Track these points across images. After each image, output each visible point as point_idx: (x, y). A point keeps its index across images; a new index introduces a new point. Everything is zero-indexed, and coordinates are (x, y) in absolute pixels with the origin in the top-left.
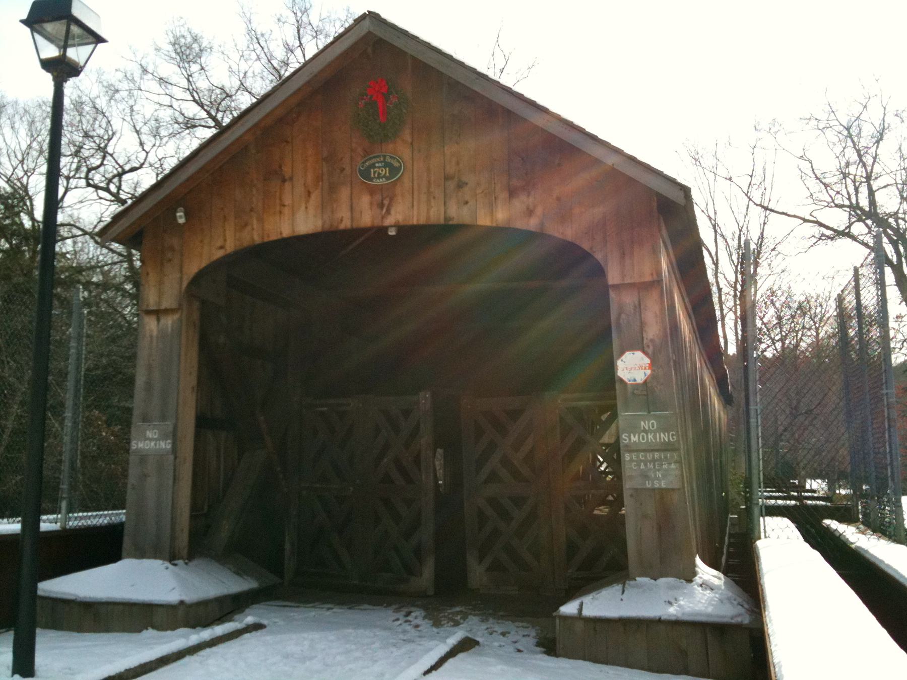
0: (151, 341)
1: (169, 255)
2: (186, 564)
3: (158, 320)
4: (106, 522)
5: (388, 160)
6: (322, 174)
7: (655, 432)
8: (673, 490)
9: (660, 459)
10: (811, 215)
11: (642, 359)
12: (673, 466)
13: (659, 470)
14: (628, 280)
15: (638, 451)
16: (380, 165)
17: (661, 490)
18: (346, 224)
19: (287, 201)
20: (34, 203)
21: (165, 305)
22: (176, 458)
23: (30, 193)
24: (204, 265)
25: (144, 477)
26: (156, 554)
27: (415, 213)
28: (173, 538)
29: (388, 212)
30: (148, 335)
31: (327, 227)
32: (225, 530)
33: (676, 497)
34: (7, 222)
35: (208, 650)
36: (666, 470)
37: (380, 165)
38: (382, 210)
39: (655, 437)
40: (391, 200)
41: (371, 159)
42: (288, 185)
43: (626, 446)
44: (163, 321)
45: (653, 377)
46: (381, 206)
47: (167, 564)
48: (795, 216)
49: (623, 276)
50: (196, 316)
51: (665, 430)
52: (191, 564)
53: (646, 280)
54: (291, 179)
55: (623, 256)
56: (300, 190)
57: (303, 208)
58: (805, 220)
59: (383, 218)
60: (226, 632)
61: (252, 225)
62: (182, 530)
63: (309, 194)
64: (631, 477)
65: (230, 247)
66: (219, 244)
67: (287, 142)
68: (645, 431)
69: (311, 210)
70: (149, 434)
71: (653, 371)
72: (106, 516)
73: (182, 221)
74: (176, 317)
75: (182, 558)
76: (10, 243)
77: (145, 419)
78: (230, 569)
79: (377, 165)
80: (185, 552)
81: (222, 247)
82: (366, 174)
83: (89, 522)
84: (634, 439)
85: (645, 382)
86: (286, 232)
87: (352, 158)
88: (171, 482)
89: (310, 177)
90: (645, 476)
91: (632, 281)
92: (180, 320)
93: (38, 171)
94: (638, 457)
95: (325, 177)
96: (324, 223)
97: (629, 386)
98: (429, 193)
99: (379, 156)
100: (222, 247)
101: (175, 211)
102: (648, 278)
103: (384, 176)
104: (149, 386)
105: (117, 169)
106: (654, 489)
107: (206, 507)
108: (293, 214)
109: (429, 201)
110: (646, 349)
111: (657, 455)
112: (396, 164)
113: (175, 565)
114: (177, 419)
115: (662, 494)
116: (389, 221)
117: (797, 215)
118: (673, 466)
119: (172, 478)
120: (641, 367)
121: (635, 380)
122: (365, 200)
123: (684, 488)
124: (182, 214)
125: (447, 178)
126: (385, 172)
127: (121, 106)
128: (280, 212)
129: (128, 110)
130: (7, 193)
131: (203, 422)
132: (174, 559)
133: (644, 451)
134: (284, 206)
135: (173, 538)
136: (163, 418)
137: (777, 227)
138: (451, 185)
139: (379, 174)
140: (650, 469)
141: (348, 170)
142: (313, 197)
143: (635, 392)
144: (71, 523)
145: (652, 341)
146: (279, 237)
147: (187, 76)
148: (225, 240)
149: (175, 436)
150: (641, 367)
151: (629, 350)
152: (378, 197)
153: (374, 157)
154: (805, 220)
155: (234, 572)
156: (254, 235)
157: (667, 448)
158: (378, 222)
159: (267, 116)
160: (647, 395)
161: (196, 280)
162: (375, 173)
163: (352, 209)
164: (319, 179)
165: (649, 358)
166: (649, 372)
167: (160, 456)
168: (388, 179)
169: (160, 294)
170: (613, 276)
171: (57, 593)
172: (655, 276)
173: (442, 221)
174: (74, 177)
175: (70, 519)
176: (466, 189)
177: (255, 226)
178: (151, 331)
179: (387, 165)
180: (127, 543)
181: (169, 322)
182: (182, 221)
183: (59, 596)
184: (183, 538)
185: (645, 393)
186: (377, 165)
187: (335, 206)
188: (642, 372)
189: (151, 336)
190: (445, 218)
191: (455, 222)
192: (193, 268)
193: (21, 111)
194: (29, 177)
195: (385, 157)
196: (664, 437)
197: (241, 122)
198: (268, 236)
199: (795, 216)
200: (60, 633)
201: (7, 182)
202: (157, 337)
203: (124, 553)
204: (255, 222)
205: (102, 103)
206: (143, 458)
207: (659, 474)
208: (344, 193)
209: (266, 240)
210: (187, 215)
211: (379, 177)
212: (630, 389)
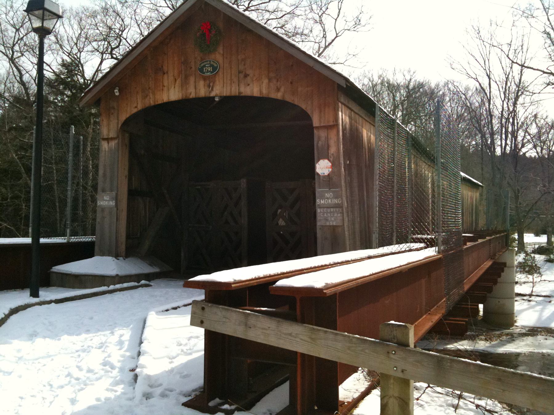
0: (105, 154)
1: (112, 111)
2: (124, 259)
3: (108, 143)
4: (90, 240)
5: (212, 63)
6: (182, 71)
7: (332, 199)
8: (339, 226)
9: (333, 212)
10: (547, 69)
11: (328, 163)
12: (339, 215)
13: (333, 217)
14: (322, 125)
15: (324, 208)
16: (208, 65)
17: (333, 226)
18: (193, 96)
19: (166, 84)
20: (84, 68)
21: (111, 135)
22: (117, 209)
23: (82, 62)
24: (128, 116)
25: (103, 218)
26: (109, 254)
27: (225, 90)
28: (117, 247)
29: (212, 89)
30: (104, 150)
31: (184, 97)
32: (146, 245)
33: (340, 229)
34: (69, 79)
35: (118, 292)
36: (336, 217)
37: (208, 65)
38: (209, 88)
39: (332, 201)
40: (214, 83)
41: (203, 62)
42: (166, 76)
43: (319, 205)
44: (110, 144)
45: (332, 172)
46: (209, 86)
47: (114, 259)
48: (538, 70)
49: (320, 122)
50: (127, 141)
51: (336, 198)
52: (126, 259)
53: (331, 124)
54: (167, 72)
55: (320, 112)
56: (171, 78)
57: (173, 87)
58: (544, 72)
59: (210, 92)
60: (129, 286)
61: (150, 96)
62: (122, 243)
63: (176, 80)
64: (320, 220)
65: (140, 107)
66: (135, 105)
67: (165, 54)
68: (327, 198)
69: (177, 87)
70: (105, 198)
71: (332, 169)
72: (90, 238)
73: (117, 94)
74: (116, 141)
75: (122, 257)
76: (71, 92)
77: (104, 191)
78: (147, 263)
79: (207, 66)
80: (124, 254)
81: (136, 107)
82: (201, 70)
83: (81, 240)
84: (322, 202)
85: (329, 174)
86: (165, 100)
87: (195, 62)
88: (115, 221)
89: (176, 71)
90: (327, 220)
91: (325, 125)
92: (118, 143)
93: (85, 49)
94: (324, 211)
95: (183, 72)
96: (183, 95)
97: (321, 177)
98: (231, 80)
99: (207, 61)
100: (136, 107)
101: (115, 89)
102: (331, 123)
103: (210, 71)
104: (104, 175)
105: (128, 48)
106: (330, 226)
107: (139, 234)
108: (168, 90)
109: (231, 84)
110: (330, 158)
111: (332, 210)
112: (215, 65)
113: (118, 259)
114: (117, 191)
115: (334, 228)
116: (213, 94)
117: (539, 69)
118: (339, 215)
119: (115, 219)
120: (327, 168)
121: (324, 174)
122: (202, 83)
123: (344, 225)
124: (117, 91)
125: (240, 72)
126: (210, 69)
127: (129, 10)
128: (163, 90)
129: (133, 12)
130: (68, 63)
131: (132, 194)
132: (118, 257)
133: (327, 208)
134: (164, 86)
135: (117, 247)
136: (111, 191)
137: (528, 76)
138: (242, 76)
139: (208, 70)
140: (329, 216)
141: (193, 68)
142: (177, 82)
143: (324, 179)
144: (72, 240)
145: (333, 154)
146: (162, 102)
147: (143, 4)
148: (138, 104)
149: (116, 199)
150: (327, 168)
151: (322, 159)
152: (208, 82)
153: (205, 62)
154: (544, 72)
155: (149, 264)
156: (151, 101)
157: (339, 206)
158: (207, 95)
159: (154, 41)
160: (329, 181)
161: (126, 123)
162: (205, 70)
163: (195, 88)
164: (180, 73)
165: (331, 163)
166: (330, 170)
167: (111, 208)
168: (212, 72)
169: (109, 131)
170: (316, 123)
171: (63, 271)
172: (335, 122)
173: (237, 94)
174: (105, 53)
175: (71, 239)
176: (249, 78)
177: (151, 97)
178: (105, 148)
179: (212, 66)
180: (96, 248)
181: (113, 144)
182: (117, 94)
183: (64, 272)
184: (123, 247)
185: (328, 180)
186: (207, 66)
187: (187, 86)
188: (327, 170)
189: (105, 151)
190: (239, 93)
191: (243, 95)
192: (123, 117)
193: (75, 13)
194: (80, 53)
195: (210, 61)
196: (336, 201)
197: (141, 45)
198: (157, 101)
199: (538, 70)
200: (65, 289)
201: (68, 56)
202: (108, 151)
203: (95, 254)
204: (151, 94)
205: (119, 7)
206: (103, 210)
207: (333, 219)
208: (192, 80)
209: (156, 103)
210: (119, 91)
211: (207, 72)
212: (321, 178)
